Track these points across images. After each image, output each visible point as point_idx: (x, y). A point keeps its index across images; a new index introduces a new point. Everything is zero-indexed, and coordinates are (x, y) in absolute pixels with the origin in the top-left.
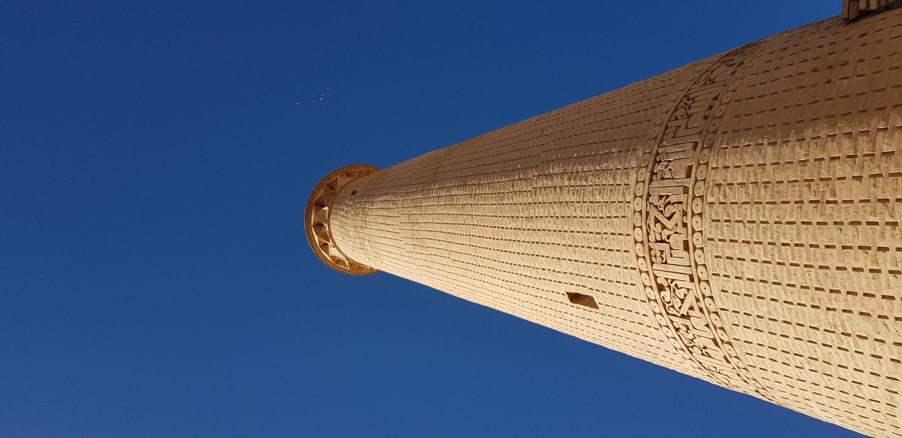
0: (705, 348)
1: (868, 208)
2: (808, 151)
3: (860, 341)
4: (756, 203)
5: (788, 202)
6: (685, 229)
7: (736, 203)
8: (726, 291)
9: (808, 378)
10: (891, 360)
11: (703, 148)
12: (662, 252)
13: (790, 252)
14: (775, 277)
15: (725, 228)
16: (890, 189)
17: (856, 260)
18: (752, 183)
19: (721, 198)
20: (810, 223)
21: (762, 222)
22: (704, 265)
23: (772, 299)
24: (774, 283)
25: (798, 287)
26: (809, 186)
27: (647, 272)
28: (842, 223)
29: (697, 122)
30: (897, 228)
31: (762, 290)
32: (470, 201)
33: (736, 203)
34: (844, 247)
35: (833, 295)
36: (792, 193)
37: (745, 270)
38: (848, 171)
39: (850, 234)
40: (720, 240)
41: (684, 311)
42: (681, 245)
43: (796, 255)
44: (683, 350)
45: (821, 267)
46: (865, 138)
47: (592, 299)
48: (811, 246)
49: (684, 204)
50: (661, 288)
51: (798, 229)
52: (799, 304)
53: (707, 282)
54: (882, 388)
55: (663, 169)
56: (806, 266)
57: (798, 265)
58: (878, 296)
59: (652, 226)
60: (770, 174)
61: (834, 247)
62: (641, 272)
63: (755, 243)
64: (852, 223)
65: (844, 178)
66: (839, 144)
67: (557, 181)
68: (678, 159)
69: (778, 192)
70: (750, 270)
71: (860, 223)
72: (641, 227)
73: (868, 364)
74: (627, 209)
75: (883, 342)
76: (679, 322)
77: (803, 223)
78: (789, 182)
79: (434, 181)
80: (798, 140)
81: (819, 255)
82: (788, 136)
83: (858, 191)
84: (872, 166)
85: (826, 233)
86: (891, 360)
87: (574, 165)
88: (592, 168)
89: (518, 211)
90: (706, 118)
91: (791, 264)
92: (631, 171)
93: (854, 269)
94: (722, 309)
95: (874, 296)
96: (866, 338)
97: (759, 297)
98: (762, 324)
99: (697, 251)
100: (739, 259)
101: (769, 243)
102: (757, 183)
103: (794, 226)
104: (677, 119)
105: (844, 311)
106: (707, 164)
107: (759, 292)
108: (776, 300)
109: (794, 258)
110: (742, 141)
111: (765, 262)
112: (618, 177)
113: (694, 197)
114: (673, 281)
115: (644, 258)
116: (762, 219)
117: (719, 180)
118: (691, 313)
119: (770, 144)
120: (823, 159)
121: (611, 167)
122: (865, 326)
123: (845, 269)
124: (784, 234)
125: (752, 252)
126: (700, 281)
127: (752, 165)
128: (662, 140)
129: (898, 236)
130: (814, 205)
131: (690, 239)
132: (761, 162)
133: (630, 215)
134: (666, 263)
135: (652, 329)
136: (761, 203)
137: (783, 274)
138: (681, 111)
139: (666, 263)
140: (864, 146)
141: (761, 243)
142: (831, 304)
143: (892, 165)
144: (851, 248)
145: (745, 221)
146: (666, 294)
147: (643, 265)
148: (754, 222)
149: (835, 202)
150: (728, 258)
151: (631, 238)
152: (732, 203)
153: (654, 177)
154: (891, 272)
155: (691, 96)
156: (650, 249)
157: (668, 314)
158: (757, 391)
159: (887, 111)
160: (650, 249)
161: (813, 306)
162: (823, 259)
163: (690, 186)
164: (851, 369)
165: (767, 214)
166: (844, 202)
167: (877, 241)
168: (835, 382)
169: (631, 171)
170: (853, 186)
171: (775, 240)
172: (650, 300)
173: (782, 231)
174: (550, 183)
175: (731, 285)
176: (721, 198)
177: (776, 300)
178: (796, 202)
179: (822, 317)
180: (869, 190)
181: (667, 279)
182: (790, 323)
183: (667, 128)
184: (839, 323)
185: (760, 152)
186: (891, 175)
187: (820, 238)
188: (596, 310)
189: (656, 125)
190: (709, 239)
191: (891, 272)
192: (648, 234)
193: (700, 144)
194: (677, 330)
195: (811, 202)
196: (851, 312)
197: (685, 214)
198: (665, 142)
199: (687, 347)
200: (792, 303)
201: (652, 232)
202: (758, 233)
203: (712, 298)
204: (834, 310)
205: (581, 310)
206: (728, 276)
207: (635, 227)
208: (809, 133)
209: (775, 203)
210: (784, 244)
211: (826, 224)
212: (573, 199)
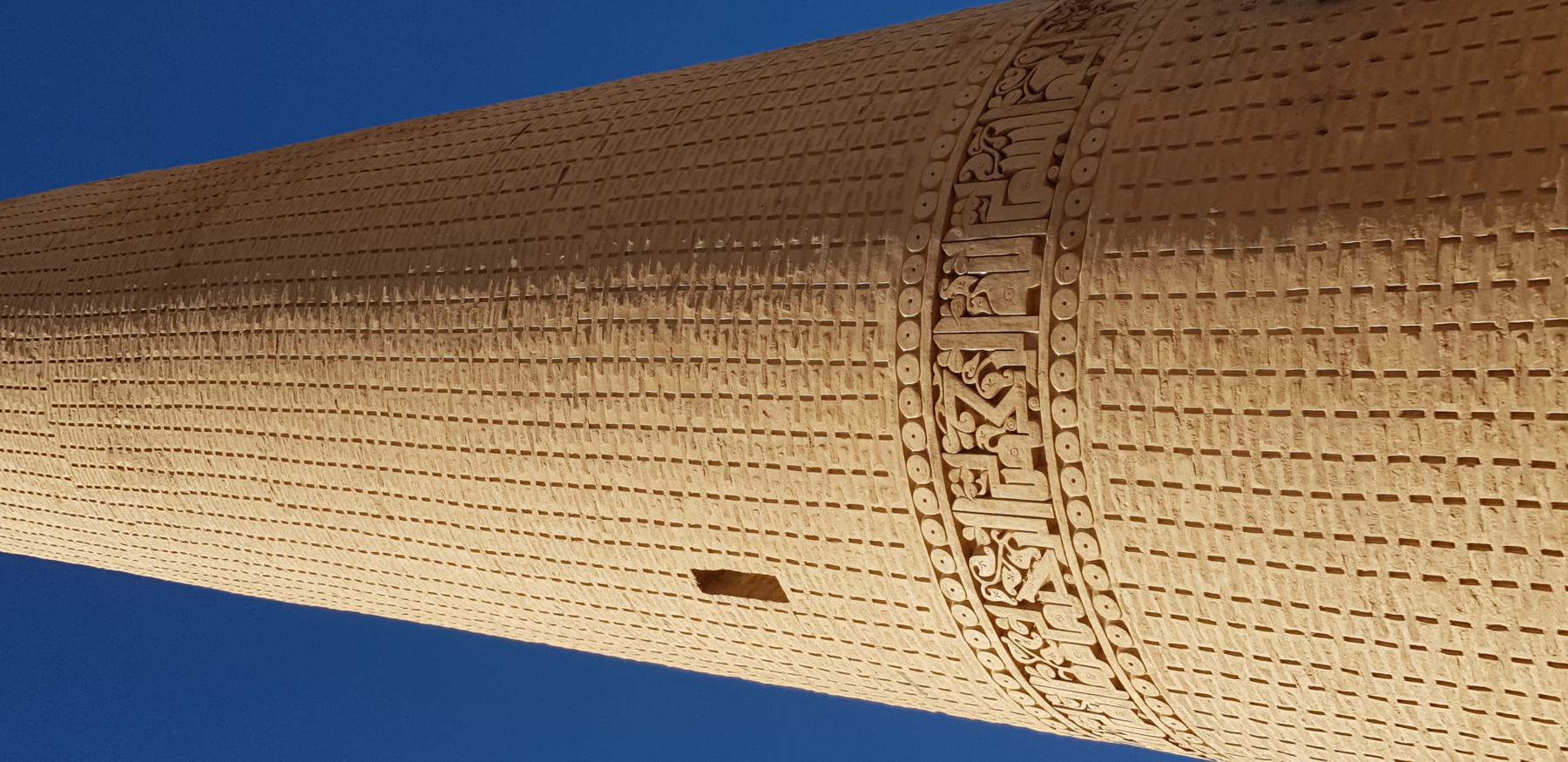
0: (1066, 664)
1: (1437, 389)
2: (1305, 274)
3: (1423, 628)
4: (1200, 373)
5: (1273, 373)
6: (1034, 424)
7: (1155, 372)
8: (1137, 550)
9: (1302, 703)
10: (1481, 656)
11: (1059, 253)
12: (977, 474)
13: (1280, 468)
14: (1250, 517)
15: (1132, 424)
16: (1476, 354)
17: (1416, 481)
18: (1186, 332)
19: (1117, 359)
20: (1322, 414)
21: (1217, 412)
22: (1085, 499)
23: (1240, 561)
24: (1246, 529)
25: (1299, 534)
26: (1315, 343)
27: (938, 518)
28: (1387, 414)
29: (1030, 189)
30: (1493, 423)
31: (1218, 543)
32: (348, 349)
33: (1155, 372)
34: (1392, 459)
35: (1372, 547)
36: (1280, 357)
37: (1182, 506)
38: (1392, 317)
39: (1405, 435)
40: (1121, 447)
41: (1028, 594)
42: (1028, 459)
43: (1295, 474)
44: (1007, 673)
45: (1346, 497)
46: (1418, 255)
47: (773, 581)
48: (1325, 457)
49: (1030, 371)
50: (970, 549)
51: (1296, 425)
52: (1299, 567)
53: (1092, 532)
54: (1456, 706)
55: (966, 292)
56: (1314, 495)
57: (1298, 494)
58: (1461, 545)
59: (951, 419)
60: (1224, 314)
61: (1372, 458)
62: (920, 517)
63: (1204, 452)
64: (1405, 414)
65: (1384, 330)
66: (1368, 265)
67: (657, 308)
68: (1001, 273)
69: (1248, 352)
70: (1190, 506)
71: (1421, 414)
72: (920, 421)
73: (1431, 666)
74: (877, 380)
75: (1467, 625)
76: (1007, 617)
77: (1306, 413)
78: (1270, 333)
79: (188, 289)
80: (1279, 250)
81: (1342, 475)
82: (1257, 238)
83: (1414, 355)
84: (1439, 309)
85: (1355, 433)
86: (1481, 656)
87: (702, 269)
88: (760, 280)
89: (536, 378)
90: (1052, 183)
91: (1284, 493)
92: (879, 295)
93: (1413, 499)
94: (1123, 585)
95: (1452, 545)
96: (1434, 621)
97: (1211, 558)
98: (1212, 610)
99: (1067, 471)
100: (1166, 484)
101: (1235, 453)
102: (1198, 332)
103: (1289, 420)
104: (973, 178)
105: (1392, 574)
106: (1074, 287)
107: (1213, 548)
108: (1251, 562)
109: (1289, 481)
110: (1153, 243)
111: (1225, 489)
112: (844, 306)
113: (1052, 359)
114: (1002, 533)
115: (930, 486)
116: (1217, 406)
117: (1108, 322)
118: (1046, 597)
119: (1217, 253)
120: (1337, 291)
121: (818, 279)
122: (1434, 600)
123: (1395, 498)
124: (1267, 435)
125: (1198, 471)
126: (1072, 531)
127: (1183, 296)
128: (948, 226)
129: (1497, 439)
130: (1328, 379)
131: (1048, 445)
132: (1203, 290)
133: (887, 394)
134: (988, 495)
135: (936, 637)
136: (1212, 373)
137: (1266, 513)
138: (980, 163)
139: (988, 495)
140: (1417, 270)
141: (1217, 453)
142: (1367, 563)
143: (1476, 309)
144: (1407, 459)
145: (1179, 409)
146: (986, 563)
147: (926, 502)
148: (1199, 411)
149: (1370, 375)
150: (1140, 483)
151: (894, 446)
152: (1144, 372)
153: (944, 311)
154: (1484, 502)
155: (999, 127)
156: (947, 468)
157: (984, 601)
158: (1167, 738)
159: (1454, 206)
160: (947, 468)
161: (1329, 570)
162: (1352, 481)
163: (1041, 334)
164: (1398, 678)
165: (1227, 395)
166: (1388, 374)
167: (1457, 447)
168: (1361, 707)
169: (879, 295)
170: (1404, 346)
171: (1248, 446)
172: (939, 575)
173: (1261, 429)
174: (634, 313)
175: (1149, 537)
176: (1117, 359)
177: (1251, 562)
178: (1289, 373)
179: (1348, 588)
180: (1436, 352)
181: (988, 530)
182: (1278, 604)
183: (953, 197)
184: (1383, 598)
185: (1199, 270)
186: (1475, 327)
187: (1343, 442)
188: (780, 606)
189: (923, 190)
190: (1094, 446)
191: (1484, 502)
192: (940, 435)
193: (1050, 243)
194: (1001, 633)
195: (1320, 373)
196: (1406, 576)
197: (1032, 392)
198: (956, 232)
199: (1021, 667)
200: (1283, 566)
201: (950, 432)
202: (1209, 434)
203: (1100, 563)
204: (1373, 573)
205: (733, 609)
206: (1143, 520)
207: (903, 421)
208: (1299, 237)
209: (1243, 374)
210: (1266, 455)
211: (1354, 415)
212: (715, 352)
